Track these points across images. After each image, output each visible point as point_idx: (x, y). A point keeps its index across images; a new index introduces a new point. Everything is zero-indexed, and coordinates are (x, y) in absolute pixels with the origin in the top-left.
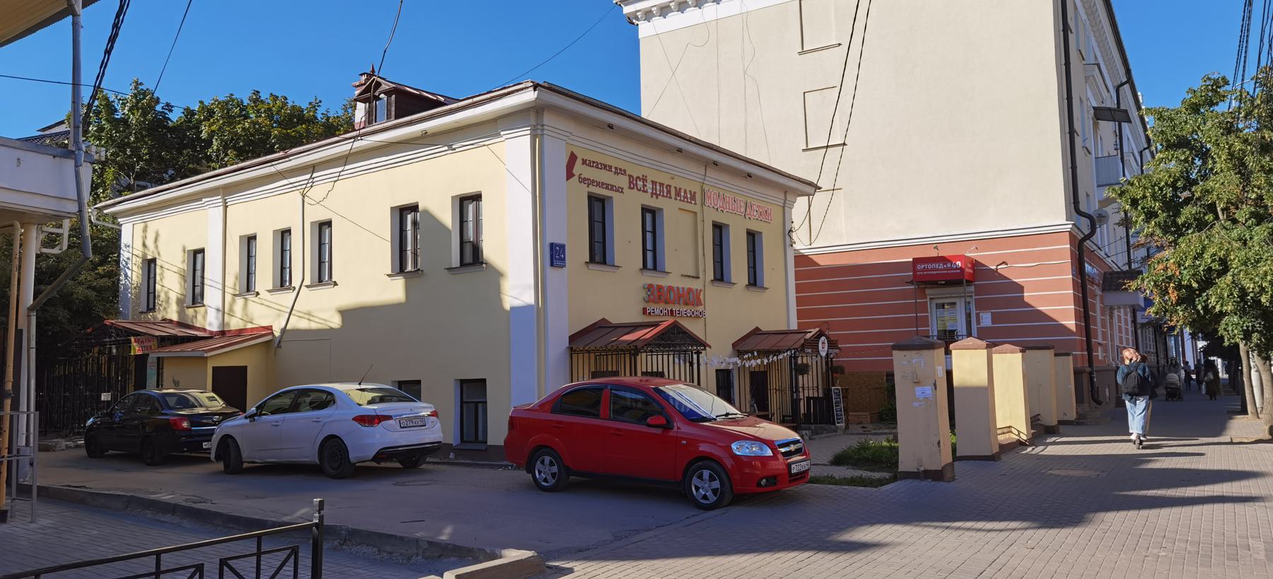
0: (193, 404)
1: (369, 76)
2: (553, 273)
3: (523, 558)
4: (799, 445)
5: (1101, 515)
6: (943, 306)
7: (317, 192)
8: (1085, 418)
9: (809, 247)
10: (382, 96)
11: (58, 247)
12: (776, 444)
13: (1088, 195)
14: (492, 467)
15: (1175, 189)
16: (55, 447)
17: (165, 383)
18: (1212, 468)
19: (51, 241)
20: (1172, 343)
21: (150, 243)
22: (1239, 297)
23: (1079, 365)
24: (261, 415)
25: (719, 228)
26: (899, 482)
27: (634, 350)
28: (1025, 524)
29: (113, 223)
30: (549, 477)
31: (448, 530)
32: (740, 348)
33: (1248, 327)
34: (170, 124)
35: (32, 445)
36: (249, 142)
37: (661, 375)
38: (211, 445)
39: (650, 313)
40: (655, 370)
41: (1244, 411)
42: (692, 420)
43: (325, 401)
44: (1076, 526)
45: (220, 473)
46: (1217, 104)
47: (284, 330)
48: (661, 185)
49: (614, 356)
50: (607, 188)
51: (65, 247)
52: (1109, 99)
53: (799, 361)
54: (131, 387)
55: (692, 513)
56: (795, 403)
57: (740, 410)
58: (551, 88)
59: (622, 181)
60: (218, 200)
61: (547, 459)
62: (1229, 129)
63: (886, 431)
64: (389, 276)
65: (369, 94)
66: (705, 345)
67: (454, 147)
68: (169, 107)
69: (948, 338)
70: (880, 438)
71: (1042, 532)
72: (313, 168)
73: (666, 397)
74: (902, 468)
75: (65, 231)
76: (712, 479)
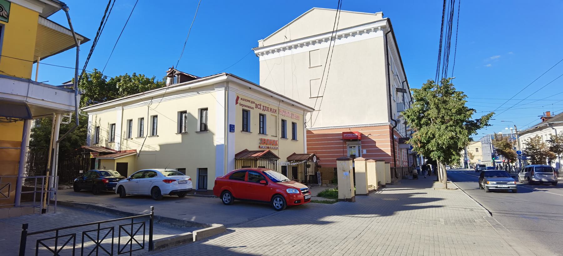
0: (110, 175)
1: (172, 69)
2: (231, 134)
3: (219, 227)
4: (307, 190)
5: (398, 212)
6: (351, 147)
7: (153, 106)
8: (393, 183)
9: (311, 128)
10: (176, 75)
11: (68, 122)
12: (301, 189)
13: (394, 114)
14: (209, 197)
15: (420, 113)
16: (63, 188)
17: (101, 168)
18: (429, 197)
19: (65, 120)
20: (418, 160)
21: (98, 122)
22: (437, 146)
23: (392, 166)
24: (132, 179)
25: (284, 122)
26: (338, 202)
27: (256, 159)
28: (376, 215)
29: (86, 114)
30: (228, 200)
31: (194, 218)
32: (289, 159)
33: (439, 155)
34: (106, 83)
35: (55, 187)
36: (131, 89)
37: (264, 167)
38: (116, 188)
39: (261, 148)
40: (262, 166)
41: (438, 180)
42: (274, 182)
43: (154, 174)
44: (391, 216)
45: (119, 197)
46: (431, 88)
47: (140, 151)
48: (266, 107)
49: (249, 161)
50: (248, 107)
51: (70, 122)
52: (400, 86)
53: (307, 164)
54: (90, 169)
55: (274, 212)
56: (306, 177)
57: (289, 178)
58: (232, 75)
59: (254, 105)
60: (121, 108)
61: (227, 194)
62: (434, 96)
63: (334, 186)
64: (176, 134)
65: (172, 75)
66: (278, 158)
67: (199, 93)
68: (106, 77)
69: (353, 157)
70: (332, 188)
71: (381, 217)
72: (152, 98)
73: (266, 174)
74: (339, 198)
75: (70, 117)
76: (280, 201)
